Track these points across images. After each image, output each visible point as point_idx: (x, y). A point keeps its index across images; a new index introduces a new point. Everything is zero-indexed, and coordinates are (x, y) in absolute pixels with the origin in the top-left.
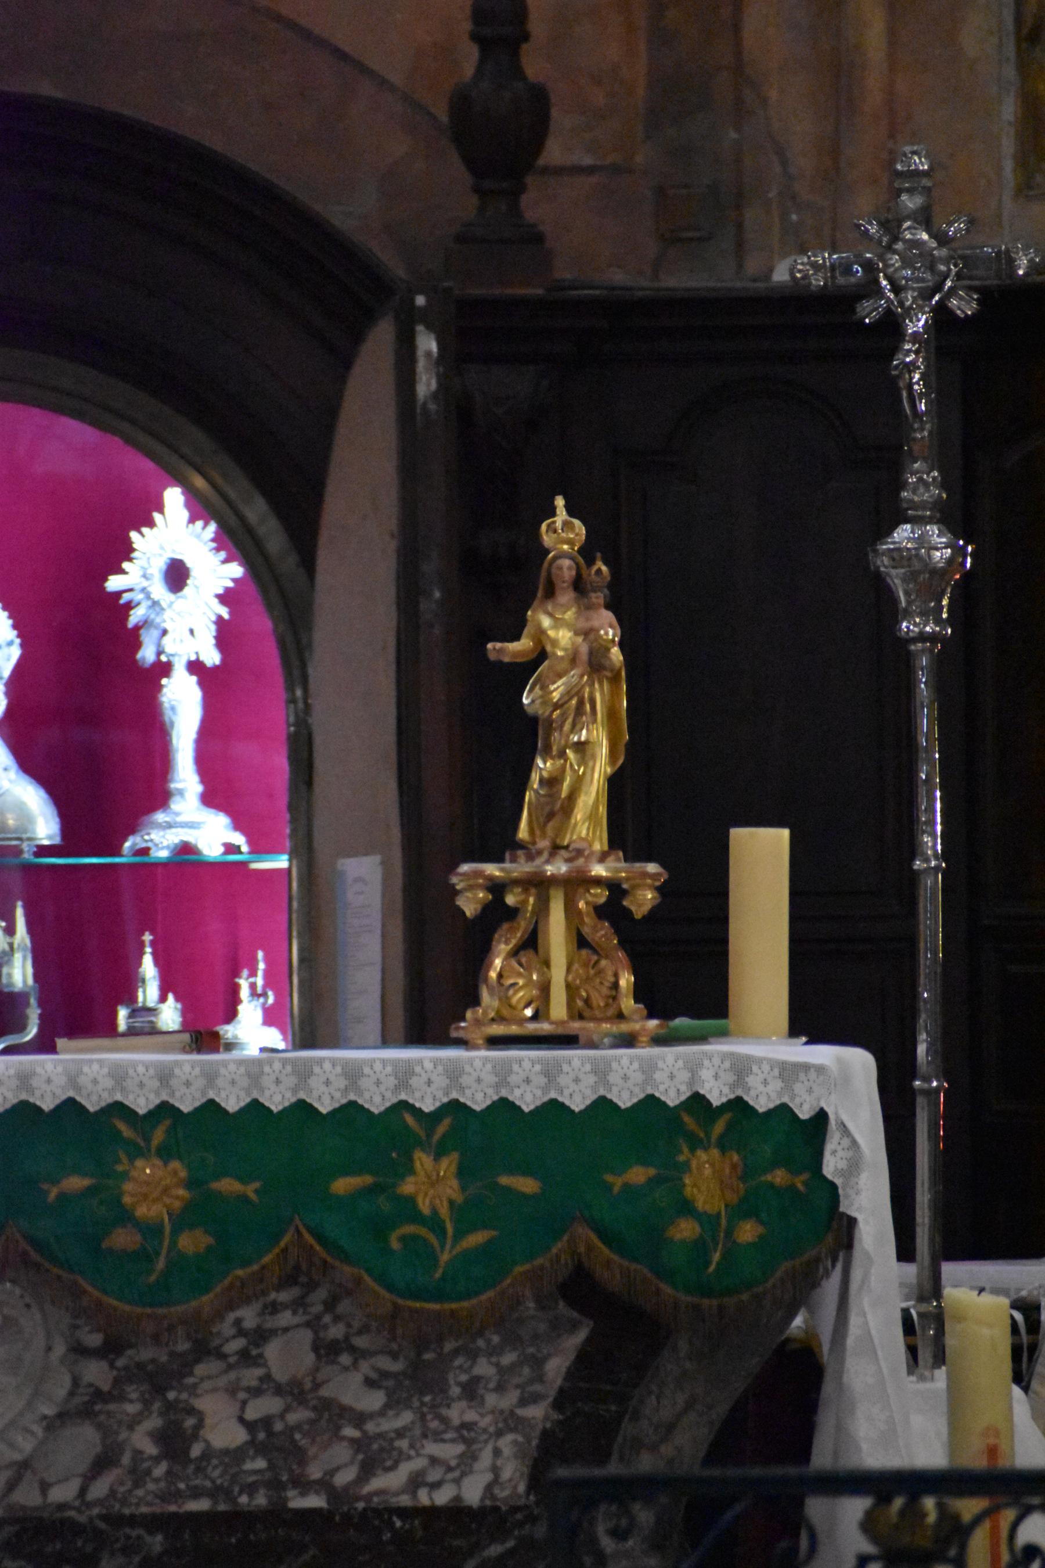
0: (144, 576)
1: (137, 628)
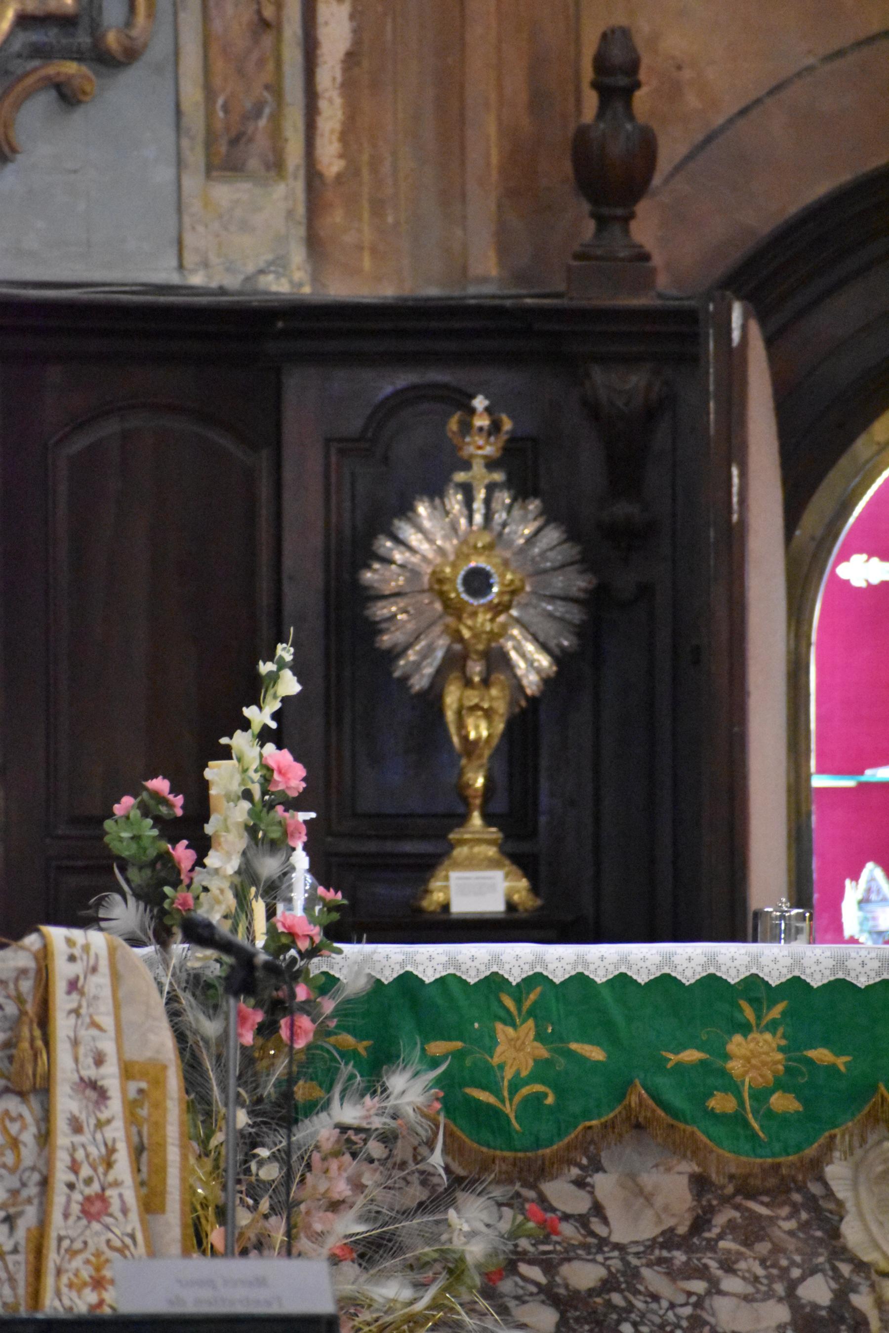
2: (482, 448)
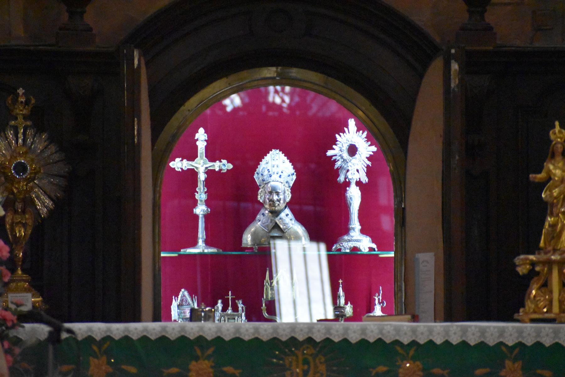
0: (341, 150)
1: (338, 169)
2: (21, 111)
